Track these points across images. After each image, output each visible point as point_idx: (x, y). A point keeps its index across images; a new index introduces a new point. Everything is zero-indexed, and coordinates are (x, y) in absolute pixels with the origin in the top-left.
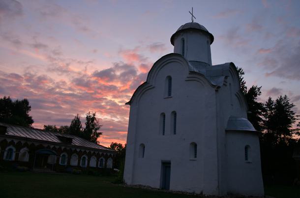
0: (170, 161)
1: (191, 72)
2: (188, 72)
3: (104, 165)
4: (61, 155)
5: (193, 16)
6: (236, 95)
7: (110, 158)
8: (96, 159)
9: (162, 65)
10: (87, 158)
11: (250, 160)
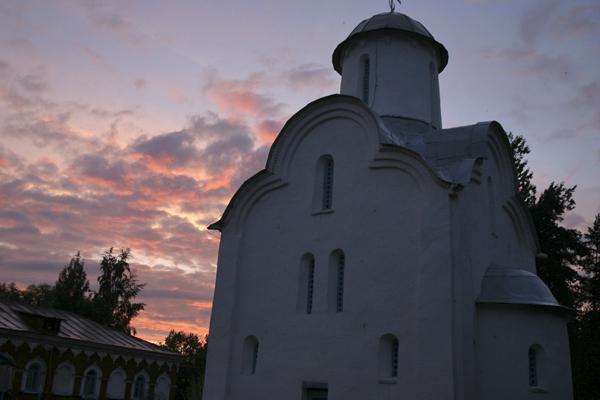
0: (326, 384)
1: (384, 145)
6: (504, 207)
8: (125, 376)
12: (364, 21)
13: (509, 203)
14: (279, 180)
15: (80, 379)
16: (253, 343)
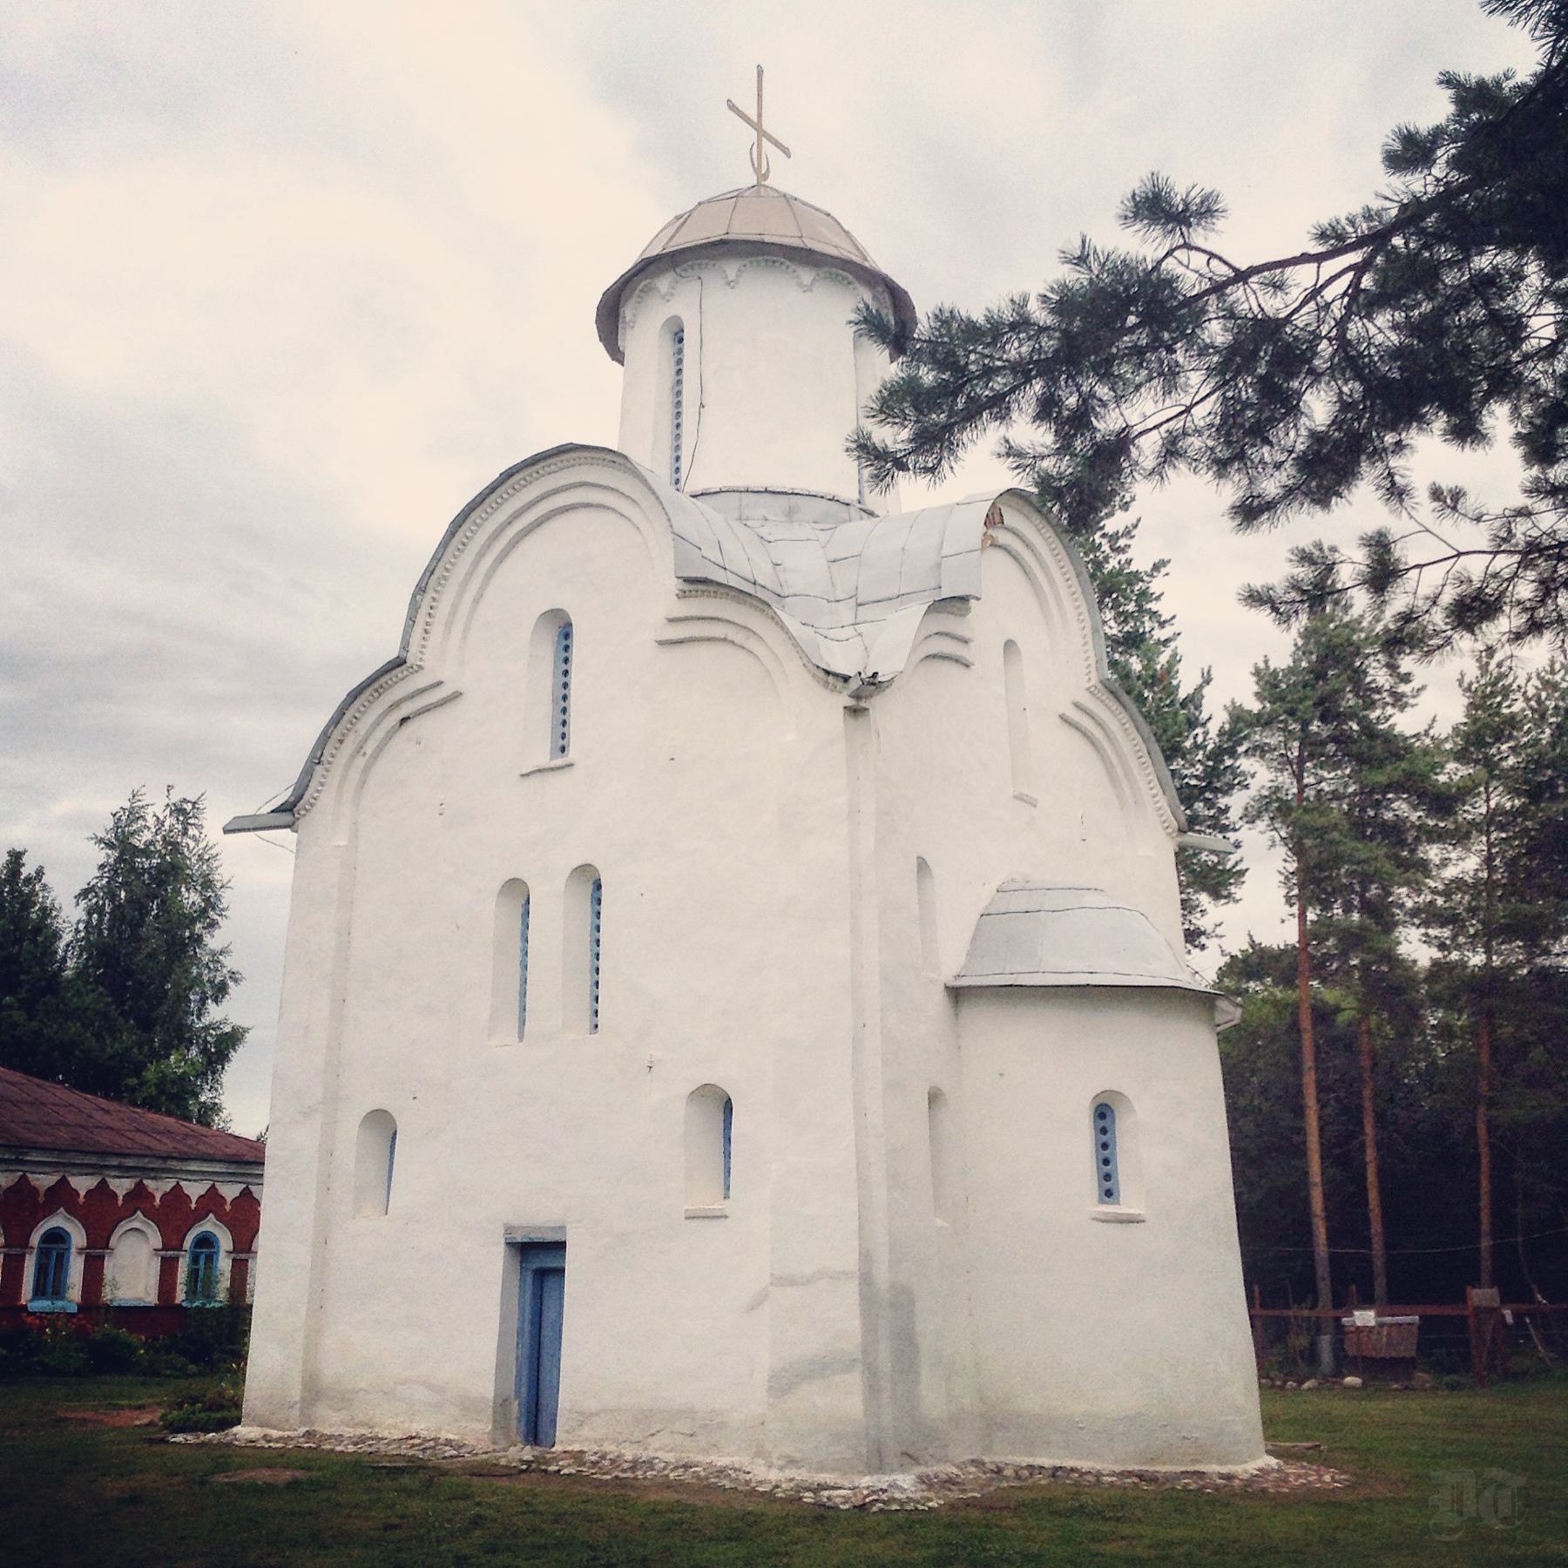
1: (687, 580)
2: (674, 585)
3: (225, 1283)
4: (35, 1239)
5: (757, 126)
6: (1065, 719)
7: (139, 1220)
8: (156, 1240)
9: (511, 532)
10: (78, 1237)
11: (1128, 1204)
12: (678, 218)
13: (1077, 705)
14: (440, 683)
15: (21, 1259)
16: (382, 1125)
